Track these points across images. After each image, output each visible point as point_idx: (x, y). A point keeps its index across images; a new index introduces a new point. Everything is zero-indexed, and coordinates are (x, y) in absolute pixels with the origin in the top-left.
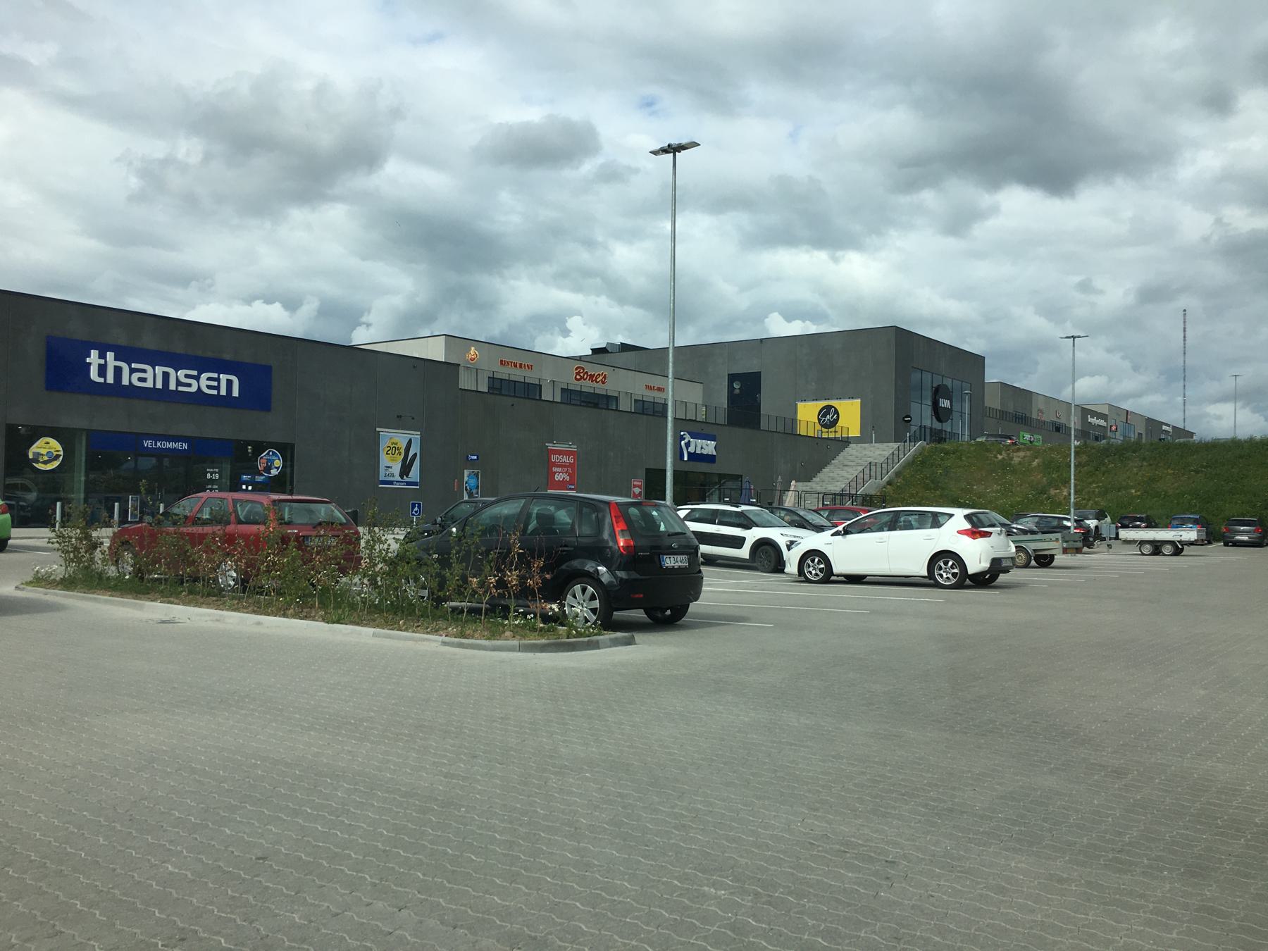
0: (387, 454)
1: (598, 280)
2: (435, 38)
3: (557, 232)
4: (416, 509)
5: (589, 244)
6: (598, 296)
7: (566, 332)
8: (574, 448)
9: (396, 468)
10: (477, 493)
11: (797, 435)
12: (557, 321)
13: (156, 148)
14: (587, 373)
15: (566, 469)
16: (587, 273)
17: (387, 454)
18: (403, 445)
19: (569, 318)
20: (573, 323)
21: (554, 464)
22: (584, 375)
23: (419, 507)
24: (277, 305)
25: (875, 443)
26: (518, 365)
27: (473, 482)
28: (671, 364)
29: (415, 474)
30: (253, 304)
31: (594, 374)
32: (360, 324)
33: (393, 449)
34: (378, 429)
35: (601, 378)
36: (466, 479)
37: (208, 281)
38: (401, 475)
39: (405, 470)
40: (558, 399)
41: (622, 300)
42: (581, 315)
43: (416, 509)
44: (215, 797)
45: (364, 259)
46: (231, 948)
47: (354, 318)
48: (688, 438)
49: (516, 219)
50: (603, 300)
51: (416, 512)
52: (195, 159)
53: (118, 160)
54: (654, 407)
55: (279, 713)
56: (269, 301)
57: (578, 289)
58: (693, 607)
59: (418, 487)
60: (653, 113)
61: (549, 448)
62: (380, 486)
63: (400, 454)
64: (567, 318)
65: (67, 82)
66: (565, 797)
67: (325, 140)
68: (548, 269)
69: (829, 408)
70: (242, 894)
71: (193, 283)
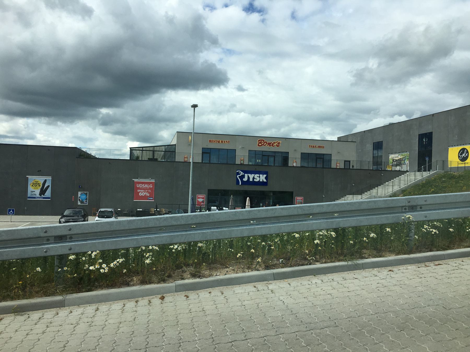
0: (32, 186)
4: (11, 211)
8: (153, 181)
9: (37, 192)
10: (86, 202)
11: (386, 170)
13: (360, 65)
14: (266, 142)
15: (147, 191)
17: (32, 186)
18: (41, 182)
21: (139, 189)
22: (264, 144)
23: (13, 210)
25: (428, 171)
26: (220, 142)
27: (84, 197)
29: (48, 193)
30: (394, 117)
31: (271, 143)
33: (36, 184)
34: (27, 176)
35: (276, 144)
36: (79, 195)
37: (377, 111)
38: (40, 194)
39: (43, 192)
45: (439, 93)
48: (242, 173)
51: (11, 213)
52: (375, 66)
53: (348, 72)
59: (50, 199)
61: (135, 181)
62: (28, 199)
63: (40, 186)
65: (332, 50)
67: (427, 49)
69: (463, 149)
71: (372, 112)
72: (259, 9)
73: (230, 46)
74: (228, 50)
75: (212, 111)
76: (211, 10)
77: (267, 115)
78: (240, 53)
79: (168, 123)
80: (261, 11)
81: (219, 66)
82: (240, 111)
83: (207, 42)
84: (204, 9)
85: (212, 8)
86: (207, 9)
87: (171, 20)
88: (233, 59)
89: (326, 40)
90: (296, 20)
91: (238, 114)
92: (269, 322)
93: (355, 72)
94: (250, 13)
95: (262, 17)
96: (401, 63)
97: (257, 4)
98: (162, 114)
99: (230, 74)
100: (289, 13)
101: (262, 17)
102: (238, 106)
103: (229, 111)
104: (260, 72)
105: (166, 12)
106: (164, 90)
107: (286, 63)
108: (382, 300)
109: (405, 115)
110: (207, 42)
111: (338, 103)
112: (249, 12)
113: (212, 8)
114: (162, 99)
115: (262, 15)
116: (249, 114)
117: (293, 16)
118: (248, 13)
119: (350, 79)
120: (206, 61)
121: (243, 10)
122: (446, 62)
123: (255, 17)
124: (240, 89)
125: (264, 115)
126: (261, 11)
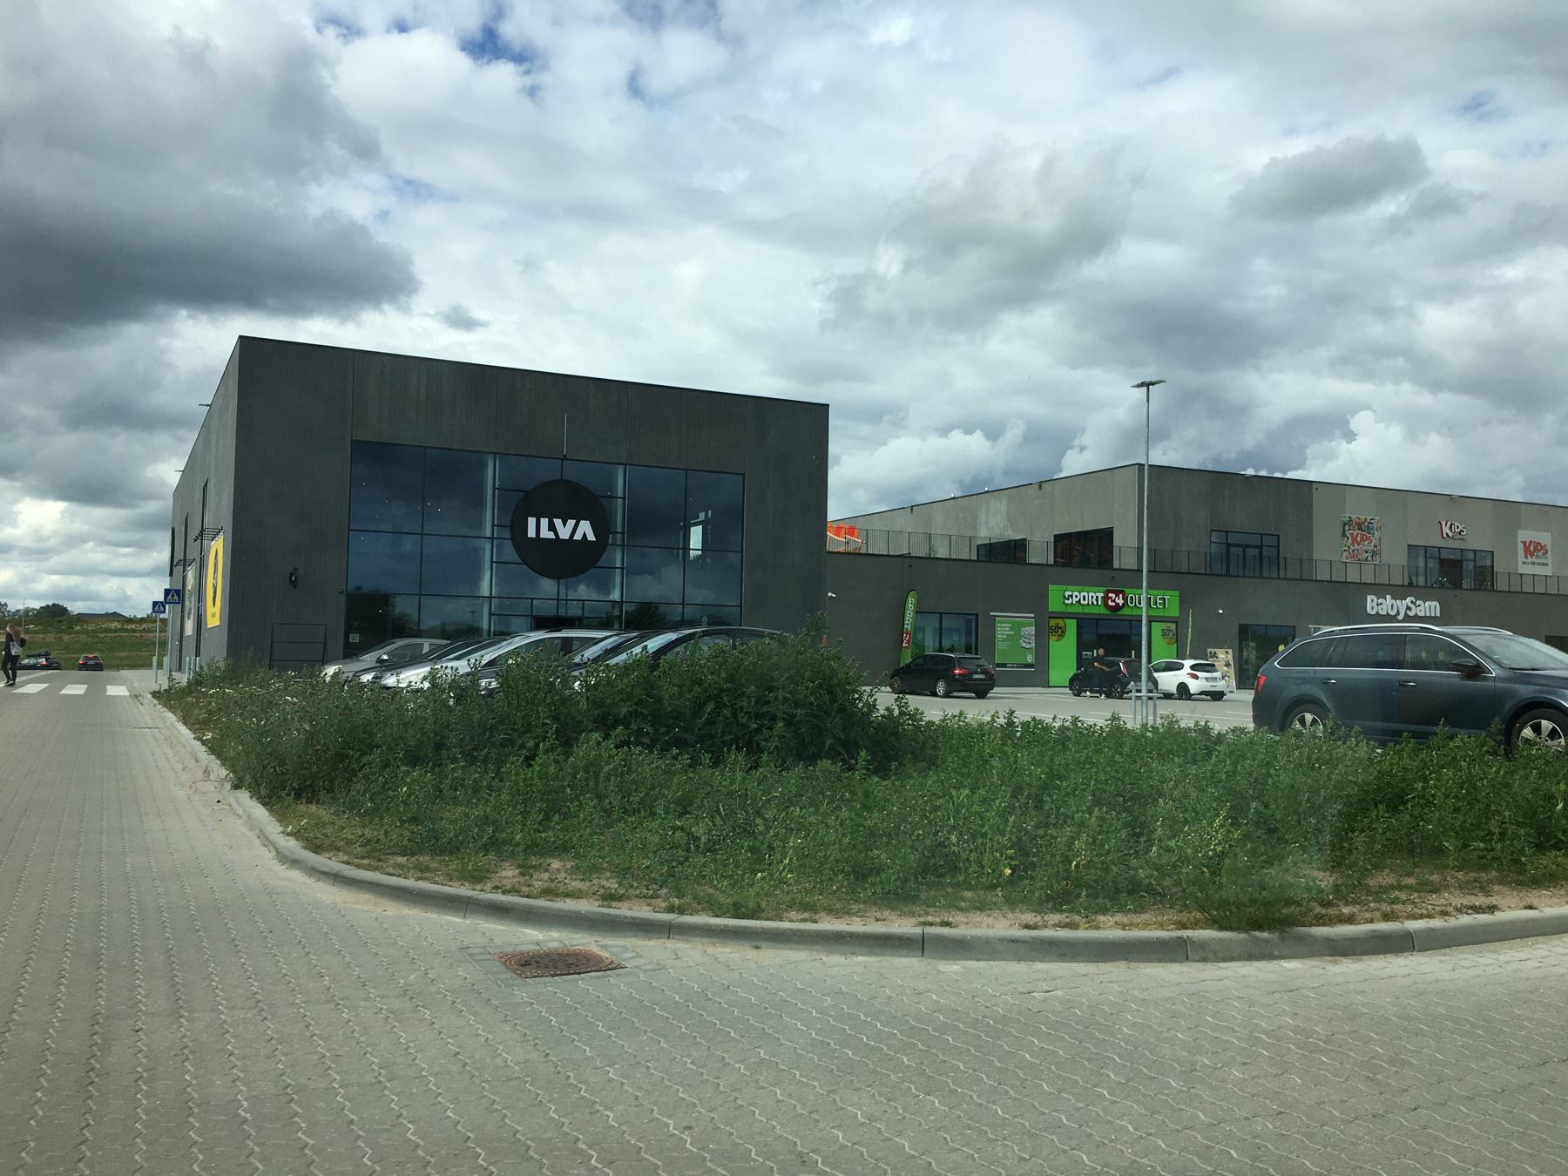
1: (1401, 362)
2: (1169, 74)
3: (1338, 299)
5: (1383, 312)
6: (1397, 383)
7: (1350, 436)
13: (851, 265)
16: (1385, 352)
19: (1352, 416)
20: (1360, 421)
24: (978, 435)
28: (1145, 508)
32: (1071, 448)
40: (974, 557)
41: (1436, 386)
42: (1368, 408)
44: (767, 988)
45: (1075, 367)
46: (1322, 1174)
47: (1059, 440)
49: (1275, 291)
50: (1406, 387)
52: (895, 270)
56: (968, 431)
57: (1367, 375)
60: (1484, 117)
64: (1349, 417)
65: (758, 208)
66: (1107, 1038)
67: (1045, 223)
68: (1323, 353)
70: (1088, 1105)
71: (886, 418)
72: (517, 49)
73: (422, 170)
74: (409, 182)
76: (345, 35)
78: (451, 198)
80: (523, 57)
81: (383, 237)
84: (319, 30)
85: (350, 30)
86: (331, 32)
87: (195, 58)
88: (427, 216)
90: (643, 99)
94: (485, 60)
95: (528, 80)
96: (971, 265)
97: (508, 30)
98: (159, 399)
99: (423, 266)
100: (619, 73)
101: (528, 80)
104: (529, 266)
106: (160, 308)
107: (612, 244)
109: (981, 430)
110: (336, 151)
112: (483, 57)
113: (348, 28)
114: (163, 341)
115: (527, 72)
117: (635, 87)
118: (479, 62)
119: (816, 305)
120: (331, 216)
121: (463, 49)
122: (1094, 270)
123: (503, 75)
126: (523, 57)
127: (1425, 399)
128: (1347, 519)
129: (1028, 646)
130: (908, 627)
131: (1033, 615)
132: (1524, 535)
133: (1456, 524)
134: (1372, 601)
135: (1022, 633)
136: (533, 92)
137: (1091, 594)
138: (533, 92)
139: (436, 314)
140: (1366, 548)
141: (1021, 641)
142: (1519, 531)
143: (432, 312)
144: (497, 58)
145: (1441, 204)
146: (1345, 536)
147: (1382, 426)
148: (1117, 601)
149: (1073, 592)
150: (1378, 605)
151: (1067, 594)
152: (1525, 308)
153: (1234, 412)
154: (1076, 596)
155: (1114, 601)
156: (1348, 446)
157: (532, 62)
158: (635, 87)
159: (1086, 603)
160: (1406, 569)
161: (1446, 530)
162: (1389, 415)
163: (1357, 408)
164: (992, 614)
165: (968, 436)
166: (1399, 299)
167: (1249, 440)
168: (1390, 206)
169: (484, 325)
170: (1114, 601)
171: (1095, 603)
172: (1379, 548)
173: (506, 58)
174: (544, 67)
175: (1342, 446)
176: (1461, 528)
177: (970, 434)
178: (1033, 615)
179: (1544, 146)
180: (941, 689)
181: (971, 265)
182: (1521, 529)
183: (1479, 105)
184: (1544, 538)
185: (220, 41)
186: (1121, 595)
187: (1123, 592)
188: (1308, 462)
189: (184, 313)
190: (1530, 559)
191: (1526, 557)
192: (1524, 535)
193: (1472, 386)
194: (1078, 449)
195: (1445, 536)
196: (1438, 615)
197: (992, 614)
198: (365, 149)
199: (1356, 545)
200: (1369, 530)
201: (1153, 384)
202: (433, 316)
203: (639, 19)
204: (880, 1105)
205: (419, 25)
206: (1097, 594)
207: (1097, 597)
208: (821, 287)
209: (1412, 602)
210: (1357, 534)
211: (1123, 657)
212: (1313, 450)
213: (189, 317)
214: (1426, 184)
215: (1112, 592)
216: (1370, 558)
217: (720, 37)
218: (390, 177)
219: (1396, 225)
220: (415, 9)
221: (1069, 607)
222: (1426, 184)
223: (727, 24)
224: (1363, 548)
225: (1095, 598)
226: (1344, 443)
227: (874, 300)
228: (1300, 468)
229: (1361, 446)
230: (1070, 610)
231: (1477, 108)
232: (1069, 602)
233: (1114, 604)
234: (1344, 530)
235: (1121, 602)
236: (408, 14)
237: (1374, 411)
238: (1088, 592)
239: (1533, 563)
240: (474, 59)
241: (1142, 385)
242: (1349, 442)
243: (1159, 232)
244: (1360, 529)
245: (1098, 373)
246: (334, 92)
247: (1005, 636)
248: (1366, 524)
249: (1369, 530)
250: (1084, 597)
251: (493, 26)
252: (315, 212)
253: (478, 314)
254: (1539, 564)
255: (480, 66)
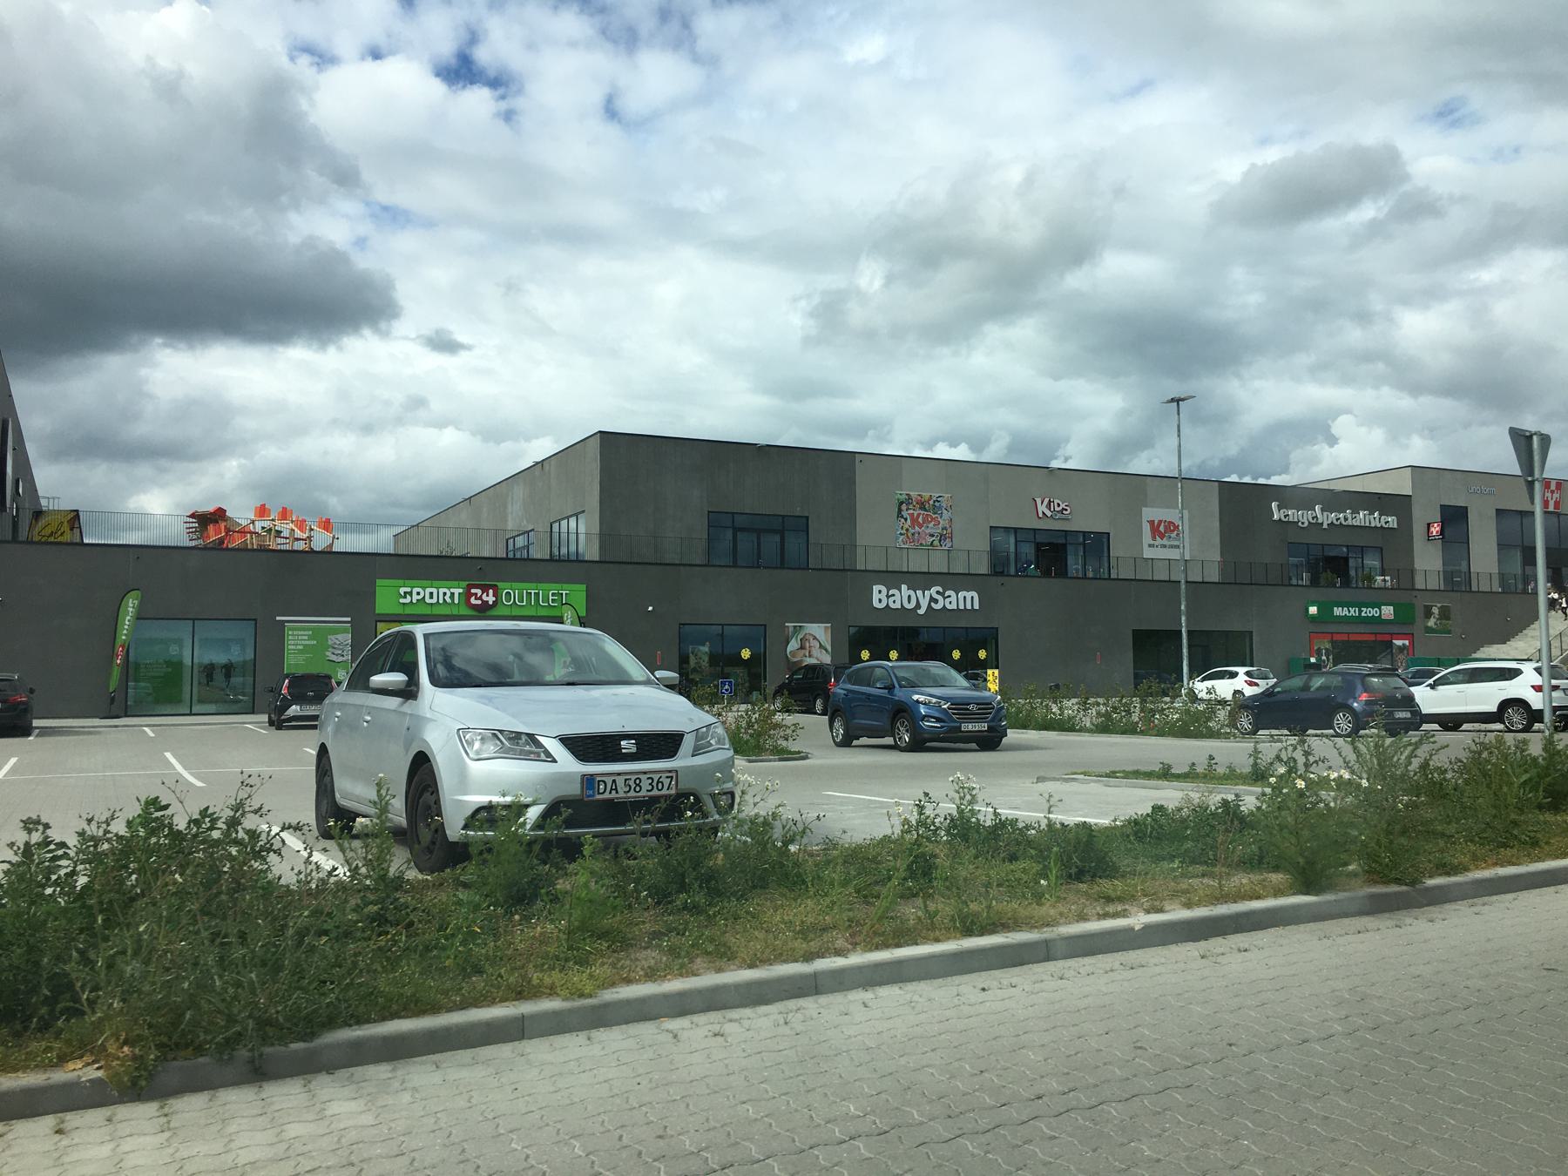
1: (1381, 366)
2: (1140, 89)
3: (1319, 306)
4: (727, 687)
5: (1363, 317)
6: (1376, 387)
7: (1332, 440)
12: (1317, 428)
13: (831, 281)
16: (1368, 357)
19: (1334, 419)
20: (1341, 425)
30: (934, 449)
41: (1416, 389)
42: (1348, 411)
43: (727, 687)
45: (1057, 378)
47: (1053, 446)
49: (1254, 299)
50: (1386, 390)
51: (727, 690)
52: (878, 284)
54: (1308, 550)
55: (1216, 1113)
57: (1347, 380)
58: (1004, 740)
60: (1456, 124)
64: (1330, 422)
65: (736, 227)
67: (1027, 234)
68: (1303, 360)
71: (871, 433)
72: (492, 73)
73: (402, 197)
74: (386, 209)
75: (335, 422)
76: (318, 64)
77: (537, 438)
78: (429, 224)
79: (163, 462)
80: (499, 82)
81: (364, 262)
82: (441, 423)
83: (314, 178)
84: (292, 59)
85: (323, 58)
86: (304, 60)
87: (169, 89)
88: (405, 242)
89: (719, 194)
90: (619, 122)
91: (433, 431)
92: (576, 1154)
93: (816, 300)
94: (460, 86)
95: (503, 105)
96: (953, 280)
97: (483, 55)
98: (141, 430)
99: (405, 292)
100: (596, 96)
101: (503, 105)
102: (437, 406)
103: (399, 421)
104: (511, 288)
105: (149, 59)
106: (135, 338)
107: (592, 266)
108: (771, 1094)
109: (967, 443)
110: (314, 178)
111: (763, 401)
112: (458, 83)
113: (321, 56)
114: (144, 372)
115: (503, 97)
116: (474, 434)
117: (611, 111)
118: (454, 88)
119: (797, 322)
120: (310, 242)
121: (438, 74)
122: (1075, 280)
123: (478, 100)
124: (443, 344)
125: (528, 439)
126: (499, 82)
127: (1405, 402)
128: (904, 497)
129: (341, 659)
130: (123, 636)
131: (349, 619)
132: (1150, 513)
133: (1056, 501)
134: (880, 592)
135: (330, 642)
136: (508, 116)
137: (442, 591)
138: (508, 116)
139: (418, 337)
140: (932, 531)
141: (327, 653)
142: (1144, 509)
143: (413, 336)
144: (472, 83)
145: (1420, 207)
146: (902, 517)
147: (1363, 430)
148: (485, 597)
149: (412, 587)
150: (888, 597)
151: (402, 590)
152: (1502, 310)
153: (1221, 419)
154: (418, 593)
155: (480, 598)
156: (1332, 450)
157: (507, 86)
158: (611, 111)
159: (434, 600)
160: (1441, 573)
161: (1042, 508)
162: (1373, 419)
163: (1336, 413)
164: (278, 618)
165: (953, 449)
166: (1376, 303)
167: (1232, 447)
168: (1368, 211)
169: (468, 348)
170: (480, 598)
171: (448, 600)
172: (949, 530)
173: (480, 83)
174: (520, 91)
175: (1325, 451)
176: (1062, 506)
177: (955, 447)
178: (349, 619)
179: (1517, 150)
180: (819, 705)
181: (953, 280)
182: (1146, 506)
183: (1451, 112)
184: (1170, 515)
185: (194, 69)
186: (491, 591)
187: (495, 588)
188: (1291, 466)
189: (159, 340)
190: (1159, 541)
191: (1154, 538)
192: (1150, 513)
193: (1452, 388)
194: (1063, 458)
195: (1041, 515)
196: (976, 606)
197: (278, 618)
198: (345, 177)
199: (916, 527)
200: (936, 509)
201: (1183, 400)
202: (413, 340)
203: (615, 42)
204: (962, 1116)
205: (392, 53)
206: (452, 590)
207: (453, 594)
208: (803, 303)
209: (938, 592)
210: (919, 515)
211: (1244, 665)
212: (1295, 455)
213: (165, 345)
214: (1406, 187)
215: (476, 587)
216: (936, 543)
217: (696, 59)
218: (367, 204)
219: (1375, 230)
220: (389, 36)
221: (434, 608)
222: (1406, 187)
223: (702, 45)
224: (928, 531)
225: (448, 594)
226: (1327, 447)
227: (857, 315)
228: (1284, 473)
229: (1342, 448)
230: (408, 611)
231: (1449, 115)
232: (408, 600)
233: (479, 602)
234: (900, 510)
235: (491, 599)
236: (381, 41)
237: (1356, 416)
238: (438, 588)
239: (1165, 546)
240: (450, 86)
241: (1173, 400)
242: (1331, 445)
243: (1136, 245)
244: (923, 507)
245: (1080, 384)
246: (313, 119)
247: (301, 647)
248: (931, 502)
249: (935, 509)
250: (431, 594)
251: (467, 52)
252: (294, 239)
253: (461, 338)
254: (1171, 547)
255: (455, 92)
